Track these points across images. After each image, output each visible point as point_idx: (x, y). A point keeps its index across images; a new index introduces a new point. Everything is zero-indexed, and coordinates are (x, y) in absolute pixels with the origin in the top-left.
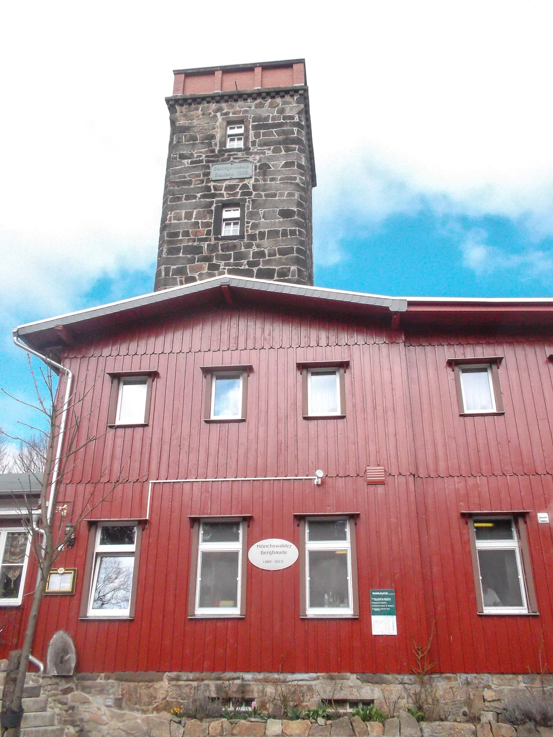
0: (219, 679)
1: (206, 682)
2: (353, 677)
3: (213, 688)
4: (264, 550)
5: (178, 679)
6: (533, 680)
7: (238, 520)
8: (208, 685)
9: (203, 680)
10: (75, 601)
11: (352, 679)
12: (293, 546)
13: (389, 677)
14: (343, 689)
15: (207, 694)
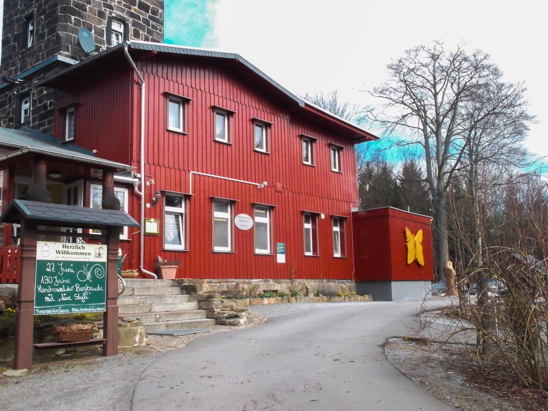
0: (227, 282)
1: (222, 284)
2: (271, 280)
3: (225, 286)
4: (241, 219)
5: (211, 282)
6: (316, 281)
7: (227, 201)
8: (223, 285)
9: (221, 282)
10: (158, 239)
11: (271, 281)
12: (251, 219)
13: (282, 280)
14: (426, 300)
15: (223, 289)
